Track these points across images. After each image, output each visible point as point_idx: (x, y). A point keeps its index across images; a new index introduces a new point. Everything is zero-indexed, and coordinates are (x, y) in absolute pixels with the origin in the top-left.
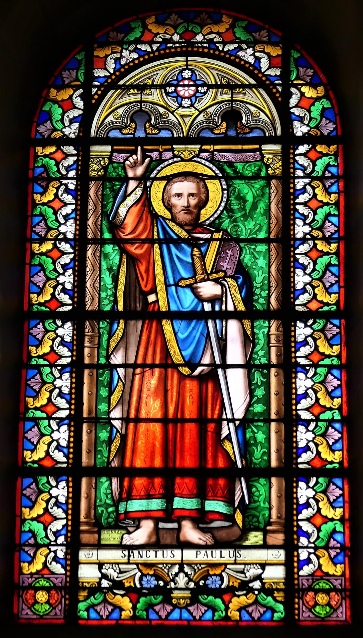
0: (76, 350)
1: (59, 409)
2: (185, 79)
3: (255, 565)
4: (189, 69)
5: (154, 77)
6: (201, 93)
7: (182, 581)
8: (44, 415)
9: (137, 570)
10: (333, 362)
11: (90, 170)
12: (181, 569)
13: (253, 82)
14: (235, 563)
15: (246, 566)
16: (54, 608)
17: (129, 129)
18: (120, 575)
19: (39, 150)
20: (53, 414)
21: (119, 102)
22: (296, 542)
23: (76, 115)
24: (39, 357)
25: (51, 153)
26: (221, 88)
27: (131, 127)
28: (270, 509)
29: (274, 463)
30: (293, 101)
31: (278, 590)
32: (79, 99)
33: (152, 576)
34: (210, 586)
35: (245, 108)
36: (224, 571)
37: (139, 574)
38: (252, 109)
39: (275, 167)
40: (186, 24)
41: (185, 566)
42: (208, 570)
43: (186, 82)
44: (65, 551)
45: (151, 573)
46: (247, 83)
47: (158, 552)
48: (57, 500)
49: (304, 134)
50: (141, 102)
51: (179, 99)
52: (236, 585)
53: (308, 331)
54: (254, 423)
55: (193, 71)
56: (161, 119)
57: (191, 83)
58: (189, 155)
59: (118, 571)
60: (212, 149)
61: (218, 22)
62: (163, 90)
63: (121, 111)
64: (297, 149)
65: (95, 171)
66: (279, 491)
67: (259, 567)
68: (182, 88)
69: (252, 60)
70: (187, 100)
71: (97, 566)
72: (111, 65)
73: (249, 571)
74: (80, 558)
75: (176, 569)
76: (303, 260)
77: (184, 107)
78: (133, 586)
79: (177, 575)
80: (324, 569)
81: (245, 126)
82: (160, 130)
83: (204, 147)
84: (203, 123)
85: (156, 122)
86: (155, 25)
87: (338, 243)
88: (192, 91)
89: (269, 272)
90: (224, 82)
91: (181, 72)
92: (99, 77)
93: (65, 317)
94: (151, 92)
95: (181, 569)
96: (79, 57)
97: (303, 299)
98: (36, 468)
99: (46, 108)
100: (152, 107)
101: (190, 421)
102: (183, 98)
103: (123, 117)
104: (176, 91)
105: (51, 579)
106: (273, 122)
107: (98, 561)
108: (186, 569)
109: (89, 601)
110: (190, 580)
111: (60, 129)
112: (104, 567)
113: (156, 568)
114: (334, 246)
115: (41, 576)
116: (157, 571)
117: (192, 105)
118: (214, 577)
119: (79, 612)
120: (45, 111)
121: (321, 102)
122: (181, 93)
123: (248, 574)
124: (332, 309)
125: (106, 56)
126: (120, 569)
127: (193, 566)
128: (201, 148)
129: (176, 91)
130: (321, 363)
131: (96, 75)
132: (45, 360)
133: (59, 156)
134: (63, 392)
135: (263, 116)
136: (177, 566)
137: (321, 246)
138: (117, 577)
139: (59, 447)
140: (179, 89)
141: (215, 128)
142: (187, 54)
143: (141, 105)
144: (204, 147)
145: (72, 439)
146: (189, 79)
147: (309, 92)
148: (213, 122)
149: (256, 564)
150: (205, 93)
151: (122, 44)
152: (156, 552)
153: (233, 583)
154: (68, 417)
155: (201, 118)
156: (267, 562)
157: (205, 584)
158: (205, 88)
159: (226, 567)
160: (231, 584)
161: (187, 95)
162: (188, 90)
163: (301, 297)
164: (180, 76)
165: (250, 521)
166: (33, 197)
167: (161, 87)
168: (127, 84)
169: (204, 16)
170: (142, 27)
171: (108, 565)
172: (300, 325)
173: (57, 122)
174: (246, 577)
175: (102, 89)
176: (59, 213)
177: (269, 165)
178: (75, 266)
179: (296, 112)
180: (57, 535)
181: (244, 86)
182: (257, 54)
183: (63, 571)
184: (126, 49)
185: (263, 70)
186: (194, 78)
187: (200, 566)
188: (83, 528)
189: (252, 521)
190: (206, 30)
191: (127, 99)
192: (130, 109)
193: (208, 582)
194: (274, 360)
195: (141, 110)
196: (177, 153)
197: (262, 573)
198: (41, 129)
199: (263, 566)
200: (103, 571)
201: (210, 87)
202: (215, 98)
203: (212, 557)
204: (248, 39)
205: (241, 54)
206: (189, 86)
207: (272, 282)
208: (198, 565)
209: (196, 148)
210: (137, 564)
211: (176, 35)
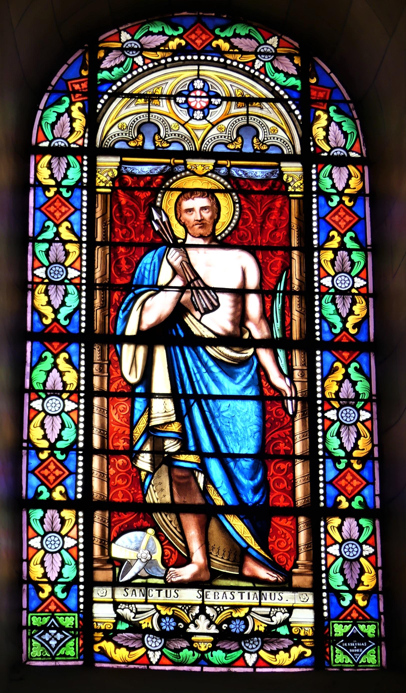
2: (195, 90)
3: (281, 609)
4: (200, 79)
5: (164, 86)
6: (214, 105)
7: (202, 622)
9: (154, 611)
12: (202, 610)
13: (271, 96)
14: (260, 606)
15: (273, 610)
17: (236, 144)
18: (137, 616)
21: (125, 112)
27: (237, 142)
31: (306, 637)
33: (170, 617)
34: (233, 630)
35: (163, 121)
36: (247, 614)
37: (157, 615)
38: (270, 125)
39: (296, 186)
41: (207, 608)
42: (231, 613)
43: (198, 93)
47: (243, 594)
55: (204, 81)
56: (170, 131)
57: (204, 94)
58: (203, 170)
59: (134, 611)
62: (172, 101)
63: (127, 121)
67: (286, 611)
68: (194, 99)
70: (199, 112)
71: (111, 605)
73: (275, 615)
75: (197, 610)
77: (196, 119)
78: (151, 628)
79: (197, 616)
81: (163, 139)
82: (170, 143)
83: (220, 162)
84: (172, 135)
85: (265, 137)
88: (204, 103)
90: (238, 94)
91: (192, 82)
95: (202, 610)
100: (161, 119)
102: (195, 110)
103: (130, 129)
104: (186, 102)
110: (212, 623)
112: (119, 607)
117: (204, 118)
122: (193, 105)
123: (274, 618)
126: (136, 609)
127: (215, 607)
129: (186, 102)
136: (198, 607)
138: (134, 618)
140: (190, 99)
141: (131, 140)
143: (248, 119)
144: (220, 162)
146: (202, 90)
148: (129, 134)
149: (283, 607)
150: (218, 106)
152: (242, 593)
153: (258, 626)
155: (215, 131)
156: (294, 605)
157: (228, 629)
158: (219, 100)
159: (250, 611)
160: (256, 629)
161: (198, 106)
162: (200, 102)
164: (191, 86)
167: (169, 97)
168: (142, 93)
171: (124, 605)
174: (272, 621)
181: (260, 100)
186: (206, 89)
188: (96, 565)
191: (133, 109)
192: (236, 122)
193: (232, 626)
195: (248, 125)
196: (190, 167)
199: (290, 610)
200: (119, 611)
201: (223, 99)
203: (271, 599)
206: (201, 97)
208: (221, 607)
209: (210, 163)
210: (155, 604)
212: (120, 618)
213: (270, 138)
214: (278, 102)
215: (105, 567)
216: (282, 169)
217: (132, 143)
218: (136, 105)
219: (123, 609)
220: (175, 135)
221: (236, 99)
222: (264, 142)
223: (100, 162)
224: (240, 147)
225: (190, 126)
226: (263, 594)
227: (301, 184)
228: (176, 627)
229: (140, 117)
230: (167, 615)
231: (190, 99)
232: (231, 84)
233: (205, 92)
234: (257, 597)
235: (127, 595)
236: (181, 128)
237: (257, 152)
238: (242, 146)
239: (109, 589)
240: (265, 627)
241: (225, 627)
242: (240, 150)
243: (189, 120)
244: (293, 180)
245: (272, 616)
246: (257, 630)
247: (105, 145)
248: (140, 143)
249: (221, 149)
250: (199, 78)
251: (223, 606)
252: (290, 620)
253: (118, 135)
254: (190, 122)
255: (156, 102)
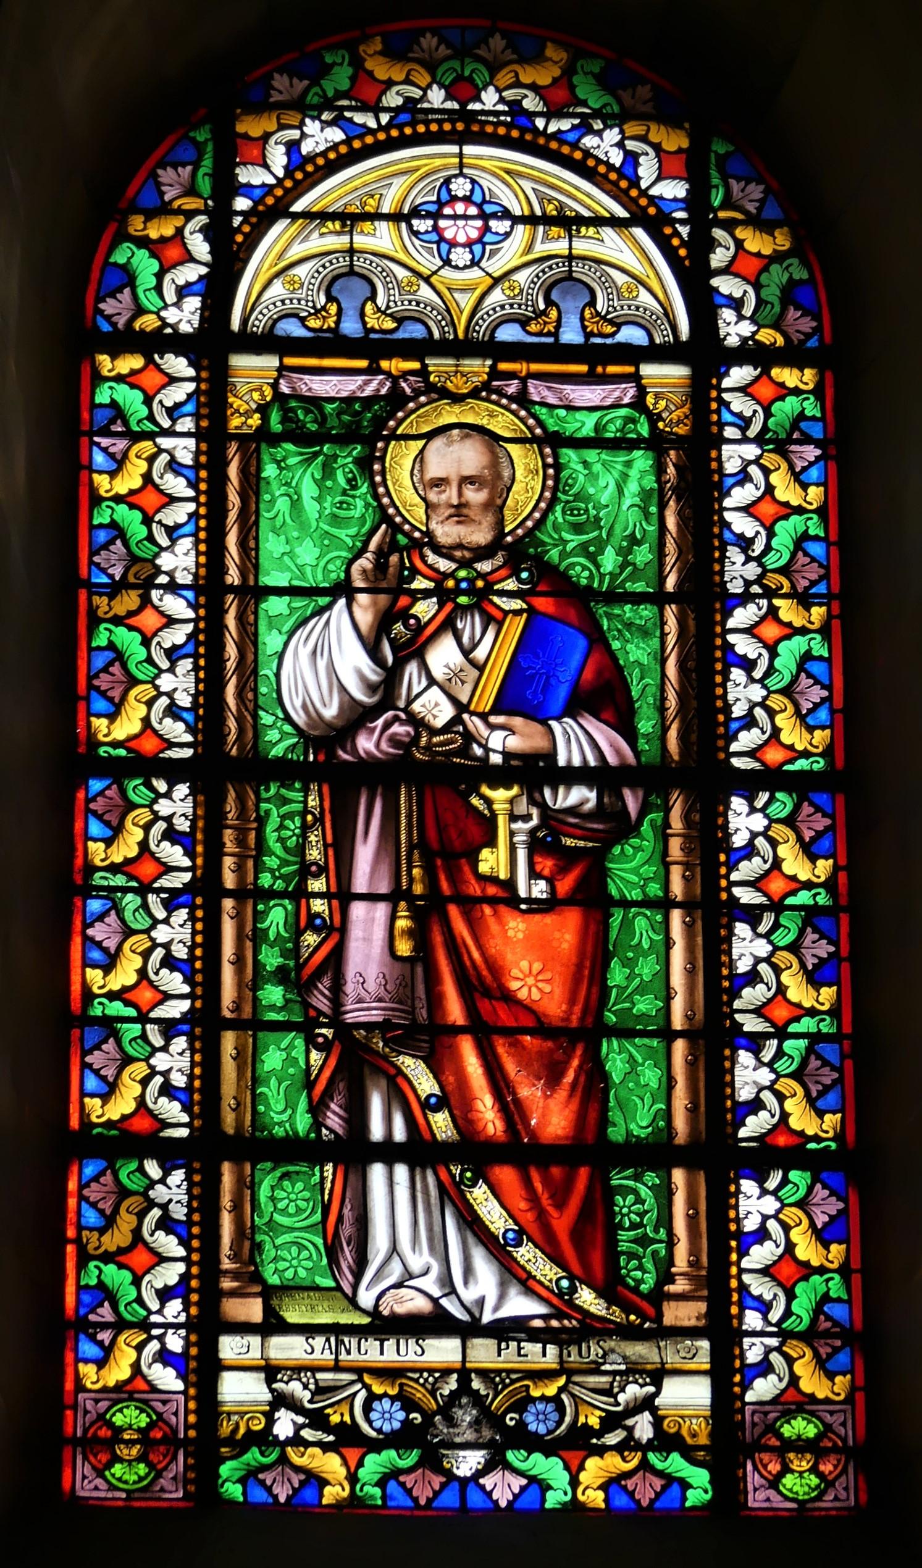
0: (208, 481)
1: (166, 997)
2: (454, 199)
4: (465, 177)
5: (384, 192)
8: (131, 1012)
9: (359, 1386)
10: (818, 898)
11: (229, 413)
13: (621, 213)
15: (618, 1378)
16: (159, 1475)
18: (317, 1398)
19: (104, 361)
20: (151, 1009)
21: (297, 251)
22: (735, 1322)
23: (193, 278)
24: (112, 996)
25: (134, 372)
26: (544, 225)
27: (547, 316)
28: (671, 1243)
29: (681, 1138)
30: (719, 258)
32: (199, 237)
36: (561, 1390)
37: (363, 1394)
38: (620, 278)
40: (456, 64)
42: (528, 1387)
43: (460, 208)
44: (193, 448)
45: (393, 1391)
46: (608, 215)
48: (171, 825)
49: (744, 340)
50: (351, 251)
51: (444, 247)
52: (594, 1421)
53: (758, 822)
54: (637, 1040)
56: (619, 300)
59: (312, 1387)
60: (524, 373)
61: (535, 58)
62: (403, 225)
64: (726, 374)
65: (241, 415)
66: (692, 1202)
67: (648, 1380)
68: (452, 222)
69: (616, 158)
70: (460, 194)
71: (262, 1376)
72: (278, 158)
74: (222, 1355)
75: (452, 1383)
76: (744, 646)
77: (456, 267)
80: (806, 1386)
81: (604, 318)
83: (503, 366)
85: (389, 301)
86: (381, 59)
87: (828, 605)
88: (472, 229)
89: (664, 675)
91: (447, 181)
92: (249, 186)
93: (174, 772)
94: (375, 230)
96: (201, 136)
97: (747, 739)
98: (114, 1137)
99: (120, 257)
101: (461, 149)
102: (453, 244)
104: (436, 228)
105: (153, 1404)
106: (666, 305)
107: (263, 1363)
108: (476, 1384)
109: (248, 1457)
111: (155, 310)
112: (279, 1376)
113: (404, 1381)
114: (818, 613)
115: (125, 1396)
116: (405, 1388)
117: (475, 263)
118: (540, 1406)
119: (222, 1486)
120: (115, 264)
121: (784, 265)
122: (448, 234)
124: (816, 767)
125: (267, 136)
126: (316, 1381)
128: (493, 367)
129: (436, 228)
130: (790, 901)
131: (243, 179)
132: (128, 1003)
133: (151, 379)
134: (180, 460)
135: (645, 297)
136: (455, 1376)
137: (787, 610)
139: (174, 709)
140: (442, 223)
142: (461, 139)
144: (503, 366)
145: (197, 1071)
146: (467, 200)
147: (756, 242)
148: (307, 301)
150: (507, 235)
151: (303, 108)
153: (586, 1417)
154: (186, 1018)
155: (497, 296)
158: (508, 223)
163: (743, 735)
165: (624, 1206)
166: (91, 481)
167: (396, 217)
168: (314, 209)
169: (497, 42)
170: (350, 64)
172: (738, 803)
173: (147, 293)
175: (254, 220)
176: (154, 643)
177: (659, 415)
178: (198, 529)
179: (726, 285)
180: (176, 414)
181: (598, 221)
182: (630, 145)
183: (179, 1386)
184: (313, 118)
185: (644, 185)
186: (477, 198)
187: (508, 1377)
189: (629, 1271)
190: (504, 77)
194: (677, 888)
195: (351, 272)
197: (657, 1393)
198: (109, 307)
202: (529, 248)
204: (604, 106)
205: (589, 141)
206: (465, 217)
207: (669, 623)
209: (477, 367)
211: (435, 87)
212: (281, 1401)
213: (622, 307)
214: (637, 226)
215: (250, 1290)
216: (643, 381)
217: (312, 321)
218: (322, 235)
219: (287, 1383)
220: (511, 306)
221: (546, 220)
222: (609, 317)
223: (649, 377)
224: (553, 330)
225: (442, 283)
226: (343, 1342)
227: (686, 417)
228: (406, 1422)
229: (550, 268)
230: (385, 1395)
231: (442, 223)
232: (536, 186)
233: (475, 204)
234: (330, 1348)
235: (423, 1352)
236: (423, 285)
237: (372, 336)
238: (338, 323)
239: (255, 1341)
240: (600, 1417)
241: (511, 1419)
242: (335, 330)
243: (440, 268)
244: (667, 408)
245: (618, 1393)
246: (583, 1424)
247: (254, 326)
248: (331, 321)
249: (509, 334)
250: (462, 174)
251: (509, 1371)
252: (657, 1402)
253: (283, 301)
254: (442, 272)
255: (367, 226)
